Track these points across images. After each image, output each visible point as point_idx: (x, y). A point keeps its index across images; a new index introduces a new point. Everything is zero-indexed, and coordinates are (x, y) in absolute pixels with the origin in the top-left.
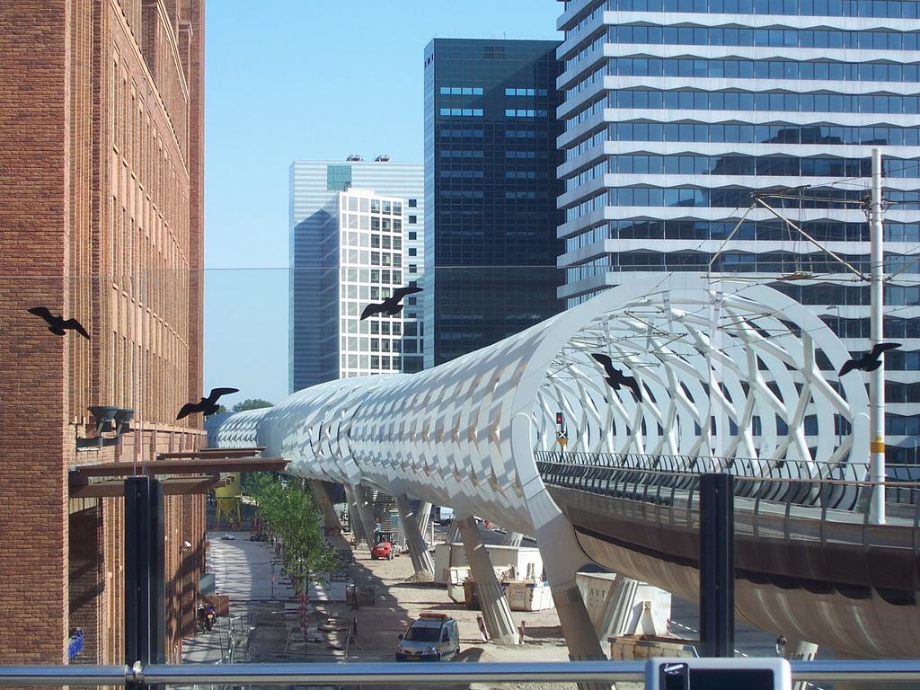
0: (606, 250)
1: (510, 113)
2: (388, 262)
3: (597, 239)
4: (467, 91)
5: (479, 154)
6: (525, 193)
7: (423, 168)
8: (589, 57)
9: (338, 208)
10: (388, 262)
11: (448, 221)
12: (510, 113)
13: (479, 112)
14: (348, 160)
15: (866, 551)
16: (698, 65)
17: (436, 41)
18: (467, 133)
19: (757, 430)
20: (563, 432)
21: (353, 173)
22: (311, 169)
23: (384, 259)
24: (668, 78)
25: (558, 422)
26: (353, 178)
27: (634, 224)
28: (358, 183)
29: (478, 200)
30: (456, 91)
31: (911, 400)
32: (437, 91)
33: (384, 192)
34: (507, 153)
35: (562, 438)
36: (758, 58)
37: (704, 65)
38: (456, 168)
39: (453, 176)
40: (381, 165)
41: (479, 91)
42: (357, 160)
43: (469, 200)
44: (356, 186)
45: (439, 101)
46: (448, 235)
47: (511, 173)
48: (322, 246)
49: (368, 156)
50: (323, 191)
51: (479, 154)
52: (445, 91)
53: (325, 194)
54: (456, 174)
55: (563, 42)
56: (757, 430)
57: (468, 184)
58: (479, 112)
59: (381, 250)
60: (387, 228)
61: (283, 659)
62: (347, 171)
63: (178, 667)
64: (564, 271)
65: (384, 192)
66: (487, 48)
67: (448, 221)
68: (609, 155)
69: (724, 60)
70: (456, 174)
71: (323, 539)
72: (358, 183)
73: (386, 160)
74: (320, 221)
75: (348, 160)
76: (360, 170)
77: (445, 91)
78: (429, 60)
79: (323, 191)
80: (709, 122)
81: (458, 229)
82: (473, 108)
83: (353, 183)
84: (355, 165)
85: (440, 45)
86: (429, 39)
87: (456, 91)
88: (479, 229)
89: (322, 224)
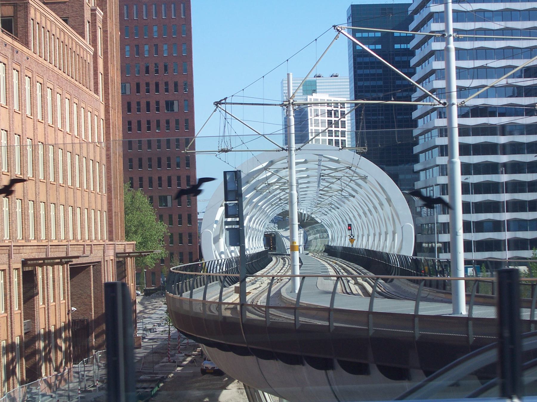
0: (436, 125)
1: (397, 46)
2: (337, 134)
3: (432, 119)
6: (407, 93)
7: (348, 80)
8: (424, 13)
10: (337, 134)
12: (397, 46)
14: (315, 77)
15: (268, 325)
16: (487, 14)
17: (352, 5)
20: (352, 235)
21: (317, 84)
22: (323, 83)
23: (335, 133)
24: (469, 23)
25: (349, 230)
26: (317, 87)
28: (320, 91)
31: (530, 210)
33: (336, 95)
34: (358, 71)
35: (352, 240)
36: (522, 9)
37: (490, 14)
38: (373, 80)
39: (365, 84)
40: (333, 79)
42: (319, 77)
44: (319, 92)
47: (399, 81)
48: (301, 127)
49: (326, 74)
50: (300, 96)
53: (301, 97)
54: (367, 83)
55: (412, 4)
59: (333, 129)
60: (337, 116)
64: (417, 137)
65: (336, 95)
66: (382, 9)
68: (436, 70)
69: (502, 11)
70: (367, 83)
72: (320, 91)
73: (336, 76)
74: (299, 113)
75: (315, 77)
76: (321, 83)
78: (349, 17)
79: (300, 96)
80: (494, 48)
82: (375, 44)
83: (317, 91)
84: (319, 80)
85: (354, 8)
86: (348, 6)
89: (300, 115)
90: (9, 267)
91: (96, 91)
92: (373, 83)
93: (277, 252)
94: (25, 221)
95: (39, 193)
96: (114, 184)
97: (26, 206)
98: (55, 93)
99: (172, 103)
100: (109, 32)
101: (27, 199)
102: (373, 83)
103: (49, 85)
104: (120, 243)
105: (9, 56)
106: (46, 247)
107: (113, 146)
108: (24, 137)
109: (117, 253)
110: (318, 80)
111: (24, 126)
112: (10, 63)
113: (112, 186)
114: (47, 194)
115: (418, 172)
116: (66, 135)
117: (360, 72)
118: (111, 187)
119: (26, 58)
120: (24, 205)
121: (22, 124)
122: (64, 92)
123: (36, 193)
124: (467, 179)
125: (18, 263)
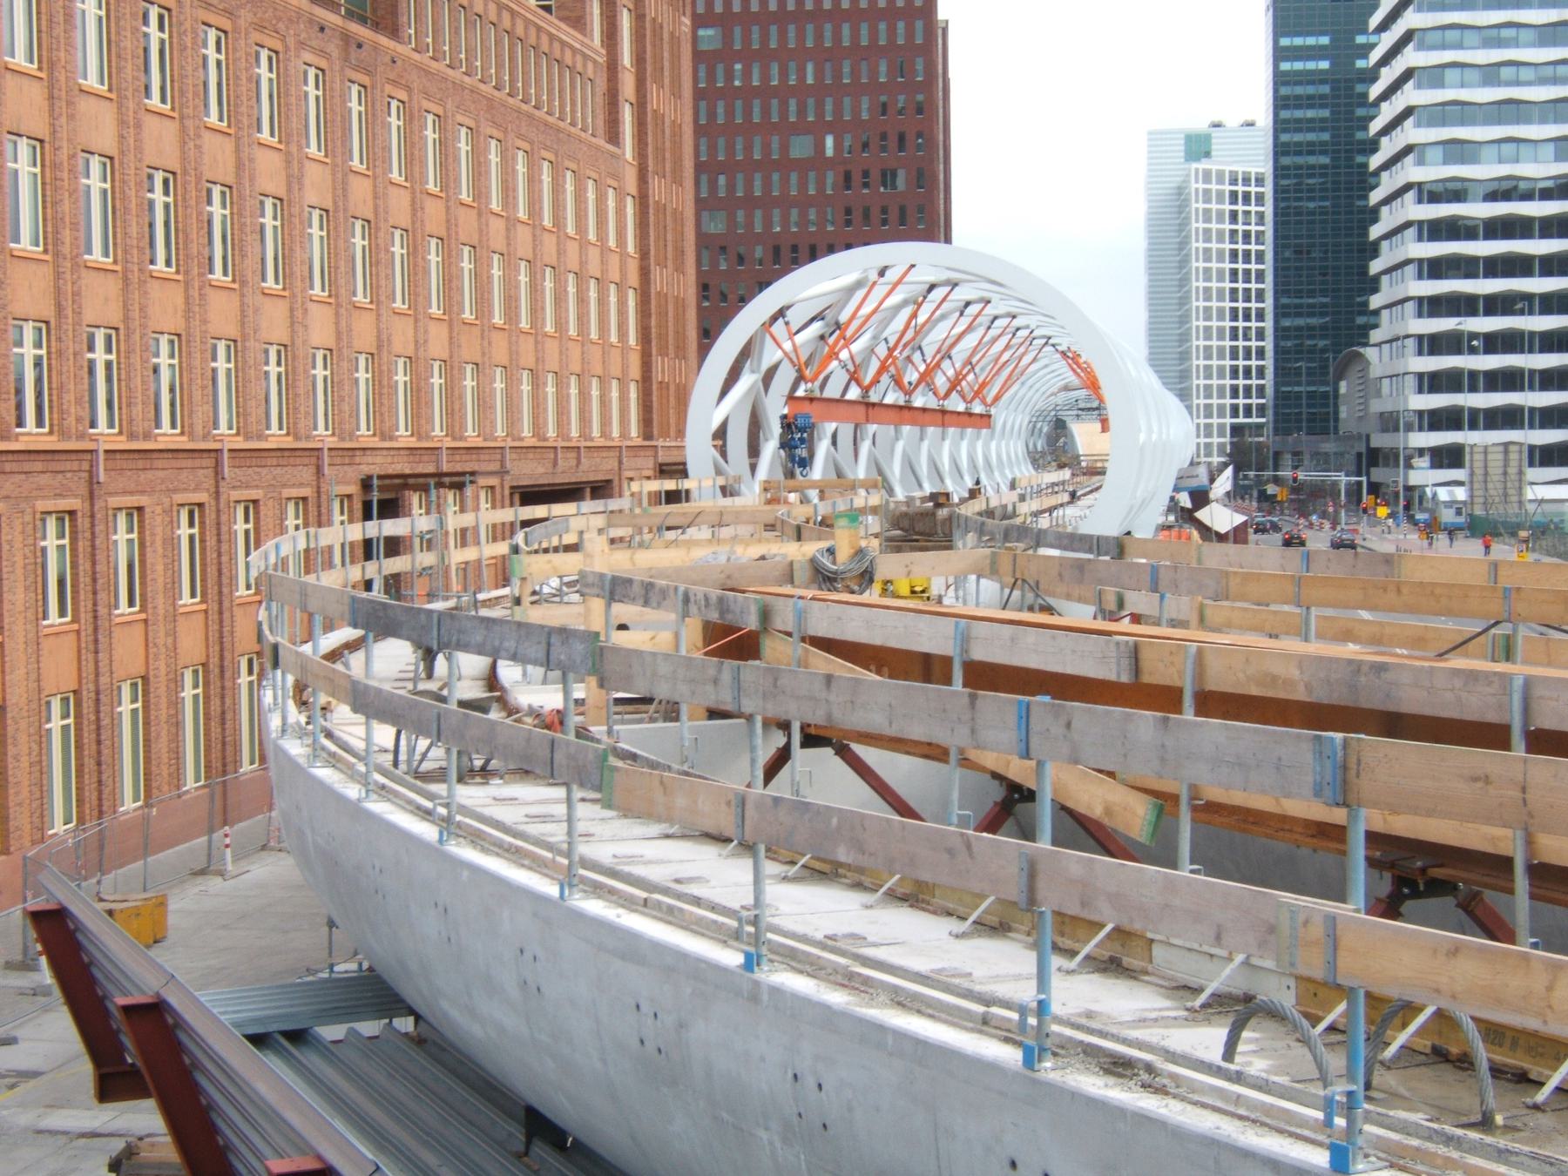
4: (1311, 41)
5: (1326, 113)
9: (1189, 181)
11: (1287, 191)
13: (1324, 65)
18: (1310, 90)
19: (394, 546)
27: (1446, 190)
29: (1324, 167)
30: (1298, 41)
32: (1276, 42)
33: (1249, 161)
38: (1310, 130)
41: (1325, 40)
43: (1313, 167)
45: (1280, 54)
46: (1288, 207)
50: (1180, 163)
51: (1326, 113)
52: (1285, 42)
54: (1298, 137)
56: (394, 546)
57: (1311, 149)
58: (1324, 65)
61: (229, 716)
62: (1207, 138)
63: (1472, 474)
64: (1376, 243)
65: (1249, 161)
67: (1287, 191)
70: (1298, 137)
71: (1019, 491)
77: (1285, 42)
79: (1180, 163)
81: (1300, 199)
83: (1213, 153)
87: (1298, 41)
88: (1323, 199)
90: (319, 492)
91: (614, 136)
92: (1311, 137)
93: (617, 478)
94: (380, 399)
95: (426, 341)
96: (659, 326)
97: (385, 368)
98: (482, 138)
99: (894, 175)
100: (648, 18)
101: (390, 353)
102: (1311, 137)
103: (460, 118)
104: (673, 444)
105: (335, 53)
106: (316, 453)
107: (657, 250)
108: (382, 225)
109: (661, 465)
110: (1215, 133)
111: (380, 202)
112: (337, 68)
113: (653, 330)
114: (451, 343)
115: (1376, 312)
116: (138, 125)
117: (1285, 114)
118: (650, 333)
119: (387, 59)
120: (380, 365)
121: (376, 197)
122: (512, 135)
123: (416, 342)
124: (1460, 324)
125: (348, 483)
